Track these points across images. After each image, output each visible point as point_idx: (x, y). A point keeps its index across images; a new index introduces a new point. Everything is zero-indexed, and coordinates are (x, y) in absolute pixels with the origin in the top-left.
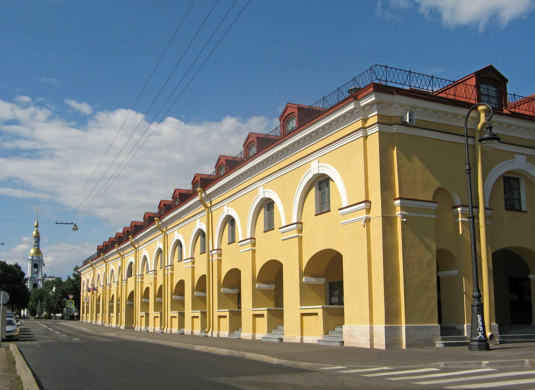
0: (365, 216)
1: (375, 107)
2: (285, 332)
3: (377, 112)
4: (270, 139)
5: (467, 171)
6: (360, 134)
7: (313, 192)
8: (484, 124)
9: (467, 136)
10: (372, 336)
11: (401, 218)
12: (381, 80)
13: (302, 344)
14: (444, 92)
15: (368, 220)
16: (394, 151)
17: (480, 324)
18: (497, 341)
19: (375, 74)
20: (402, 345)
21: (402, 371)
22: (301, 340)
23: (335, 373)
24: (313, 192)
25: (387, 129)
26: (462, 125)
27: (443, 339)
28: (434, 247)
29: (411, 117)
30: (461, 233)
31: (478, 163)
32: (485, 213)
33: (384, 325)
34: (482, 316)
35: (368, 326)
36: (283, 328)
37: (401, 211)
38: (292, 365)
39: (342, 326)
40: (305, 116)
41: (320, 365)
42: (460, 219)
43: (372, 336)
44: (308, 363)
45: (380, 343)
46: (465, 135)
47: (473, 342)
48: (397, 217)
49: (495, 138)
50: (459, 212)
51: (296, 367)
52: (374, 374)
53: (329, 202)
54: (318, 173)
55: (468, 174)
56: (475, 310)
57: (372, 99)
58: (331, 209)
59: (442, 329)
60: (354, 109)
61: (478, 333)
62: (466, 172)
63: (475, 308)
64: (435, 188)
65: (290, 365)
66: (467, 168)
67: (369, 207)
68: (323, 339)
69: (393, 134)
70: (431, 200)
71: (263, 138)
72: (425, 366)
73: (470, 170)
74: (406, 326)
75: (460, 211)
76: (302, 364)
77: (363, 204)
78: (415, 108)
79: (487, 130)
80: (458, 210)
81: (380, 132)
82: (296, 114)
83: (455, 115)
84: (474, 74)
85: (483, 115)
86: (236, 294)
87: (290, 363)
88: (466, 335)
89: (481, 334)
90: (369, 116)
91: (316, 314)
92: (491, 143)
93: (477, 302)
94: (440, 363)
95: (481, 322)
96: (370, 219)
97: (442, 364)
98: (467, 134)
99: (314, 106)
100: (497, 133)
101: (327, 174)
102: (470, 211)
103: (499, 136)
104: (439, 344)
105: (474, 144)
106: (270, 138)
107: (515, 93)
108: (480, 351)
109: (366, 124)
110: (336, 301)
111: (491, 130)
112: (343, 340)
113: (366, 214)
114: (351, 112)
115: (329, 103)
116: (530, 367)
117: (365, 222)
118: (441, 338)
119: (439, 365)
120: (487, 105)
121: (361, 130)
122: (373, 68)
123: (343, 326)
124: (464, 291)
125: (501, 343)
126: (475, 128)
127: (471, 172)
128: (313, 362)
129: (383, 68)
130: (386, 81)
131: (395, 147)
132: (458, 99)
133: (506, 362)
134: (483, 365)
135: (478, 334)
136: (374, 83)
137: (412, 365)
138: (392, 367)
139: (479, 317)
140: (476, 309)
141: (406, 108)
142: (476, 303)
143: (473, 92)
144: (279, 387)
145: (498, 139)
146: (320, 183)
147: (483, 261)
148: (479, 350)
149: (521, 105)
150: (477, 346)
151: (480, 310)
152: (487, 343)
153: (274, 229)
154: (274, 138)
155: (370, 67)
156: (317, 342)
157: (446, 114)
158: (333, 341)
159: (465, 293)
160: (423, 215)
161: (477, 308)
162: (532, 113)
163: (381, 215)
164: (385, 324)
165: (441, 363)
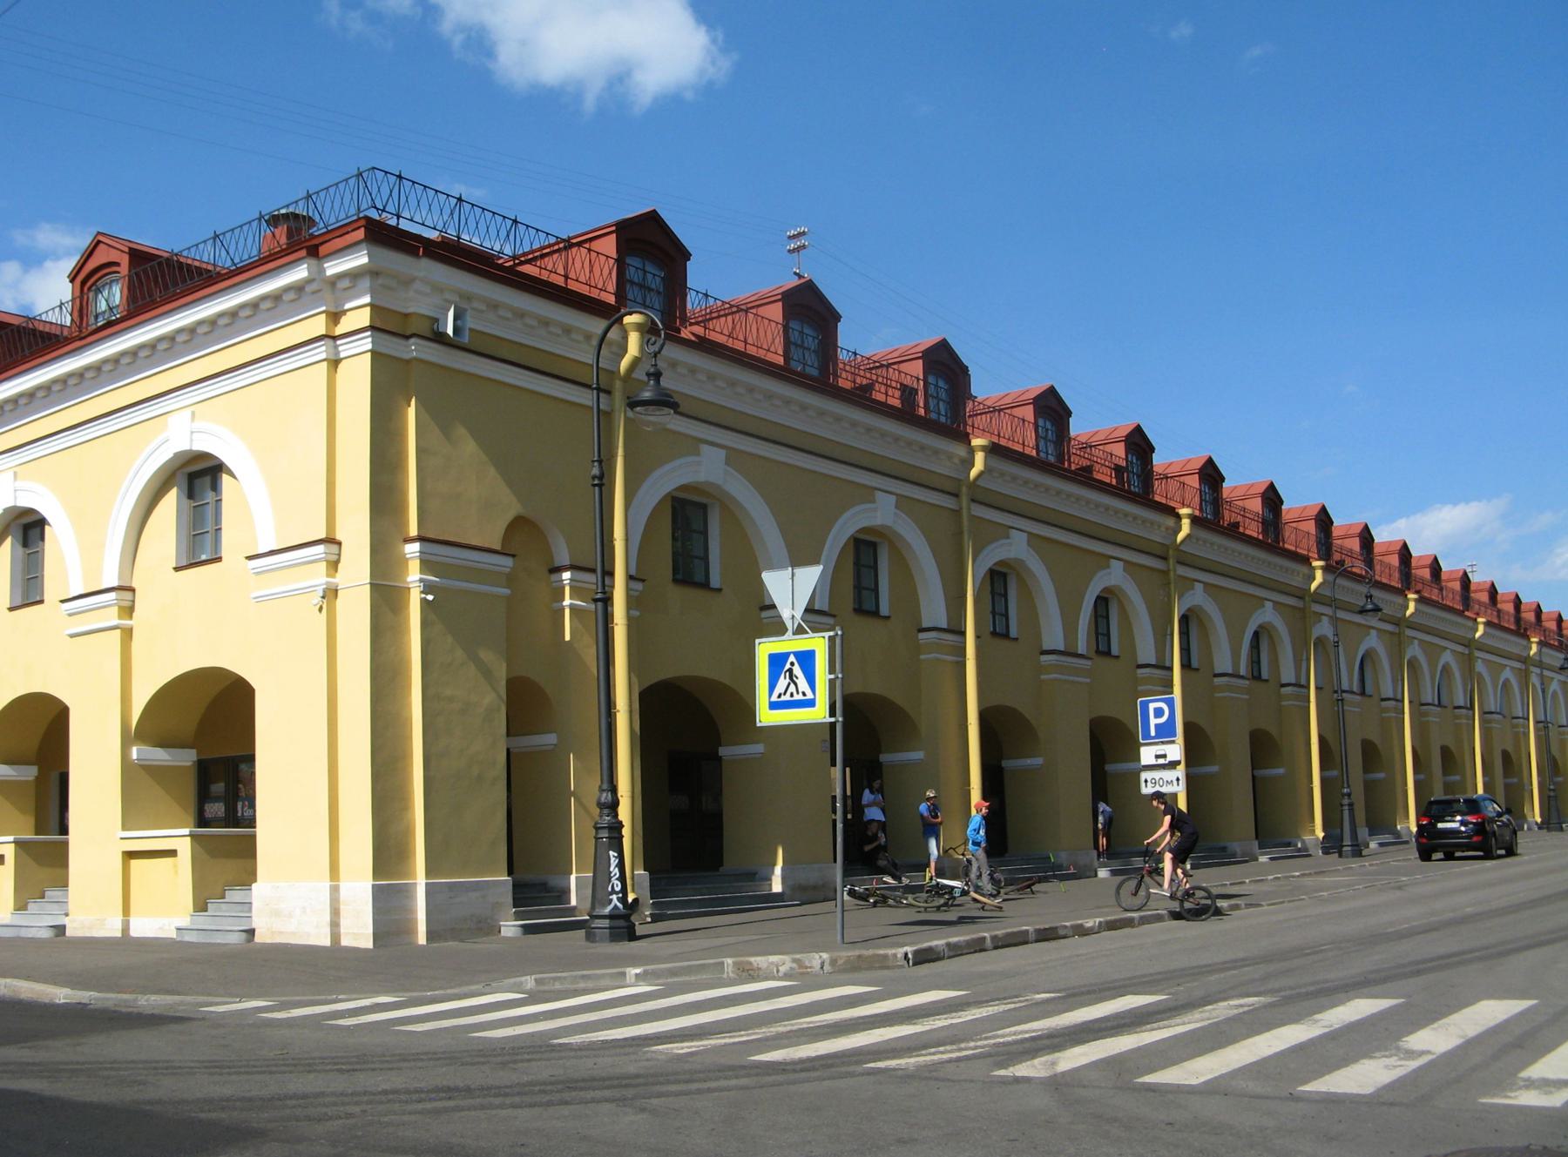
0: (324, 579)
1: (366, 283)
2: (71, 907)
3: (371, 297)
4: (41, 332)
5: (594, 480)
6: (321, 351)
7: (171, 499)
8: (636, 362)
9: (599, 390)
10: (335, 912)
11: (422, 592)
12: (383, 210)
13: (126, 942)
14: (702, 324)
15: (331, 593)
16: (409, 409)
17: (615, 874)
18: (646, 916)
19: (371, 194)
20: (417, 933)
21: (431, 1004)
22: (123, 930)
23: (251, 1022)
24: (171, 499)
25: (394, 347)
26: (589, 358)
27: (518, 916)
28: (501, 673)
29: (459, 322)
30: (567, 638)
32: (628, 590)
33: (372, 882)
34: (619, 854)
35: (326, 885)
36: (67, 897)
37: (421, 573)
38: (115, 1005)
39: (251, 886)
40: (156, 282)
41: (201, 999)
42: (567, 602)
43: (335, 912)
44: (162, 997)
45: (359, 932)
46: (594, 386)
47: (597, 921)
48: (409, 589)
49: (665, 401)
50: (565, 582)
51: (130, 1010)
52: (359, 1018)
53: (216, 535)
54: (191, 450)
55: (597, 488)
56: (602, 838)
57: (359, 259)
58: (224, 553)
59: (517, 887)
60: (308, 281)
61: (611, 897)
62: (591, 482)
63: (605, 834)
64: (510, 516)
65: (109, 1005)
66: (596, 471)
67: (335, 558)
68: (191, 924)
69: (408, 362)
70: (498, 547)
71: (18, 327)
72: (488, 989)
73: (601, 477)
74: (427, 884)
75: (568, 581)
76: (147, 1001)
77: (320, 548)
78: (469, 298)
79: (649, 380)
80: (564, 578)
81: (374, 352)
82: (124, 268)
83: (567, 330)
84: (614, 228)
85: (634, 340)
87: (108, 999)
88: (573, 902)
89: (618, 898)
90: (347, 306)
91: (172, 853)
92: (658, 413)
93: (609, 818)
94: (523, 979)
95: (617, 869)
96: (337, 590)
97: (529, 982)
98: (598, 384)
99: (185, 254)
100: (674, 391)
101: (217, 456)
102: (597, 584)
103: (676, 399)
104: (510, 928)
105: (958, 509)
106: (41, 329)
107: (400, 172)
108: (613, 943)
109: (336, 325)
110: (219, 813)
111: (658, 381)
112: (254, 926)
113: (328, 576)
114: (298, 288)
115: (231, 252)
116: (736, 977)
117: (323, 597)
118: (515, 912)
119: (521, 983)
120: (650, 314)
121: (323, 343)
122: (365, 175)
123: (254, 885)
124: (572, 789)
125: (656, 918)
126: (615, 369)
127: (603, 483)
128: (179, 994)
129: (392, 179)
130: (399, 217)
131: (412, 398)
132: (573, 286)
133: (682, 968)
134: (630, 979)
135: (611, 900)
136: (367, 218)
137: (451, 988)
138: (401, 994)
139: (614, 856)
140: (607, 835)
141: (448, 296)
143: (508, 236)
144: (106, 1073)
145: (674, 406)
146: (193, 478)
147: (618, 711)
148: (612, 941)
149: (712, 319)
151: (615, 838)
152: (630, 921)
153: (41, 602)
154: (53, 332)
155: (356, 169)
156: (173, 935)
157: (546, 323)
158: (222, 927)
159: (573, 794)
161: (609, 833)
162: (743, 344)
163: (368, 581)
164: (374, 879)
165: (529, 977)
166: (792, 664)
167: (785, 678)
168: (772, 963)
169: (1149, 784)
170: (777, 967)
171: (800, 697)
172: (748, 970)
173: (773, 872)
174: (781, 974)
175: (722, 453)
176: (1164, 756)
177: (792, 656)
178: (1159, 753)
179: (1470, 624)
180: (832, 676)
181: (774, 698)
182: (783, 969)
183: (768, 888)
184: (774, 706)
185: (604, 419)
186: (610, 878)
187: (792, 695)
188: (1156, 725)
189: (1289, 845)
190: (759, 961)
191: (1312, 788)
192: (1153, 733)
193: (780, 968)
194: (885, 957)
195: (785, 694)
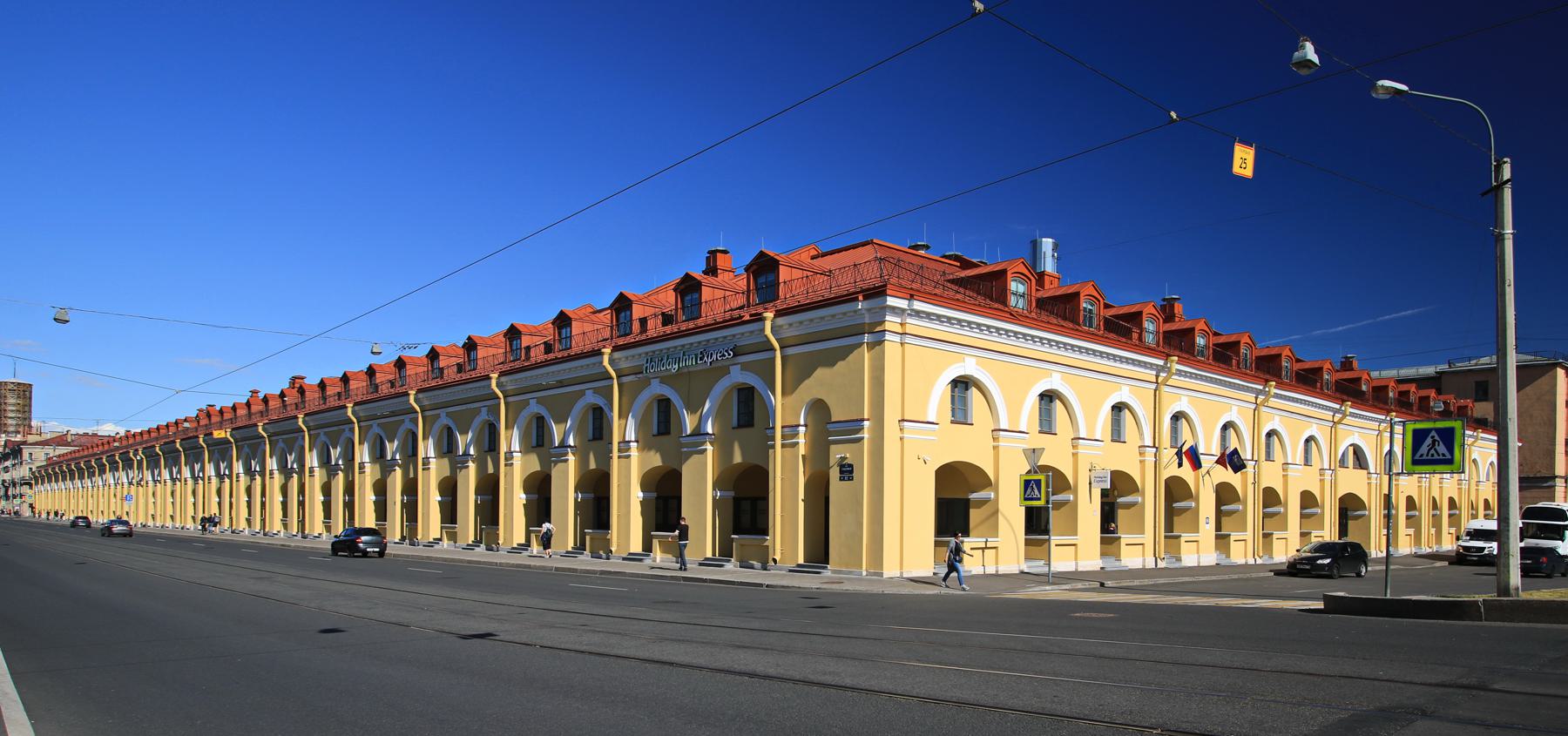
171: (1441, 457)
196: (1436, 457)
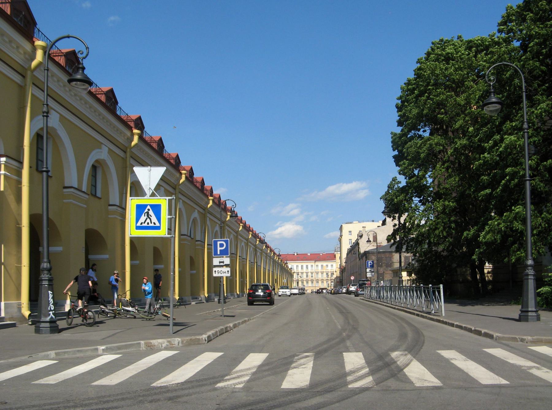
17: (51, 302)
31: (27, 108)
61: (50, 313)
62: (42, 114)
75: (4, 162)
86: (51, 246)
94: (49, 352)
95: (52, 299)
105: (23, 85)
111: (83, 71)
119: (48, 355)
133: (123, 346)
135: (50, 314)
139: (51, 293)
140: (47, 283)
142: (47, 277)
148: (51, 333)
150: (49, 328)
159: (3, 264)
160: (151, 153)
161: (48, 283)
166: (149, 210)
167: (145, 216)
168: (159, 343)
169: (216, 272)
170: (162, 344)
171: (153, 225)
172: (150, 346)
173: (65, 303)
174: (163, 348)
175: (58, 115)
176: (223, 262)
177: (149, 206)
178: (220, 261)
179: (238, 225)
180: (170, 217)
181: (139, 224)
182: (164, 345)
183: (63, 309)
184: (138, 228)
185: (22, 89)
186: (49, 303)
187: (148, 223)
188: (220, 250)
189: (196, 298)
190: (155, 342)
191: (204, 278)
192: (219, 253)
193: (163, 345)
194: (199, 339)
195: (144, 223)
196: (150, 225)
